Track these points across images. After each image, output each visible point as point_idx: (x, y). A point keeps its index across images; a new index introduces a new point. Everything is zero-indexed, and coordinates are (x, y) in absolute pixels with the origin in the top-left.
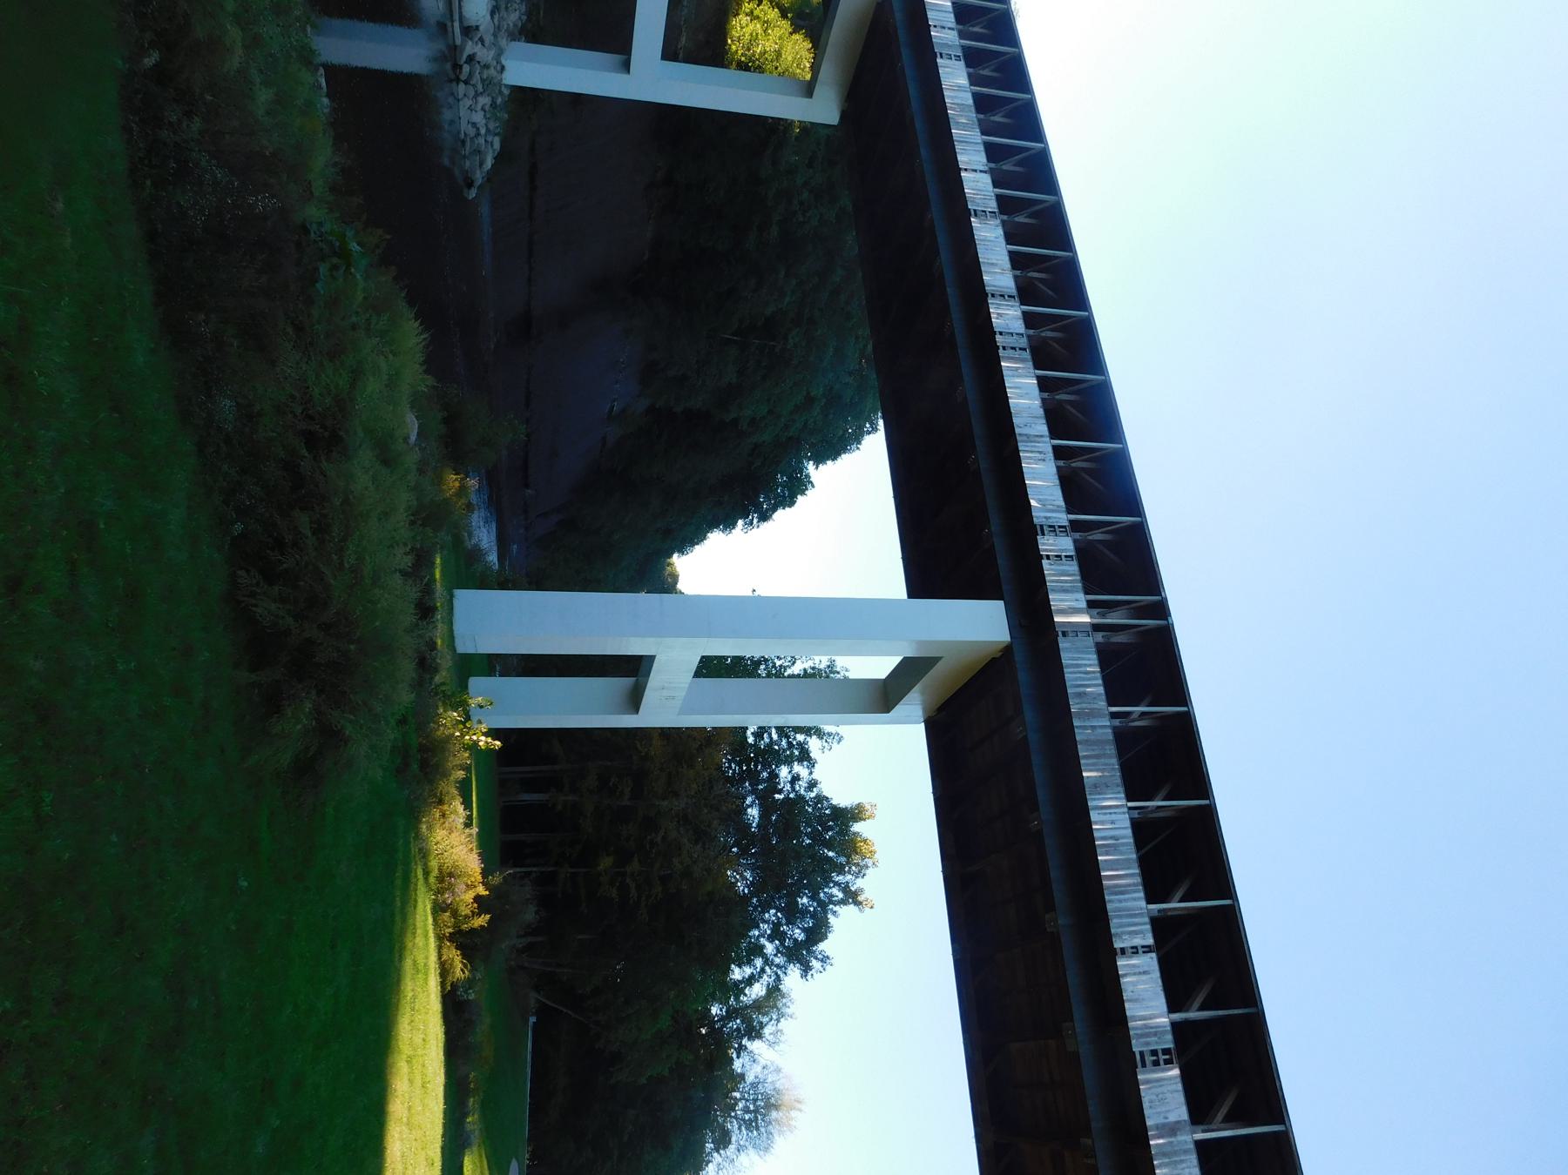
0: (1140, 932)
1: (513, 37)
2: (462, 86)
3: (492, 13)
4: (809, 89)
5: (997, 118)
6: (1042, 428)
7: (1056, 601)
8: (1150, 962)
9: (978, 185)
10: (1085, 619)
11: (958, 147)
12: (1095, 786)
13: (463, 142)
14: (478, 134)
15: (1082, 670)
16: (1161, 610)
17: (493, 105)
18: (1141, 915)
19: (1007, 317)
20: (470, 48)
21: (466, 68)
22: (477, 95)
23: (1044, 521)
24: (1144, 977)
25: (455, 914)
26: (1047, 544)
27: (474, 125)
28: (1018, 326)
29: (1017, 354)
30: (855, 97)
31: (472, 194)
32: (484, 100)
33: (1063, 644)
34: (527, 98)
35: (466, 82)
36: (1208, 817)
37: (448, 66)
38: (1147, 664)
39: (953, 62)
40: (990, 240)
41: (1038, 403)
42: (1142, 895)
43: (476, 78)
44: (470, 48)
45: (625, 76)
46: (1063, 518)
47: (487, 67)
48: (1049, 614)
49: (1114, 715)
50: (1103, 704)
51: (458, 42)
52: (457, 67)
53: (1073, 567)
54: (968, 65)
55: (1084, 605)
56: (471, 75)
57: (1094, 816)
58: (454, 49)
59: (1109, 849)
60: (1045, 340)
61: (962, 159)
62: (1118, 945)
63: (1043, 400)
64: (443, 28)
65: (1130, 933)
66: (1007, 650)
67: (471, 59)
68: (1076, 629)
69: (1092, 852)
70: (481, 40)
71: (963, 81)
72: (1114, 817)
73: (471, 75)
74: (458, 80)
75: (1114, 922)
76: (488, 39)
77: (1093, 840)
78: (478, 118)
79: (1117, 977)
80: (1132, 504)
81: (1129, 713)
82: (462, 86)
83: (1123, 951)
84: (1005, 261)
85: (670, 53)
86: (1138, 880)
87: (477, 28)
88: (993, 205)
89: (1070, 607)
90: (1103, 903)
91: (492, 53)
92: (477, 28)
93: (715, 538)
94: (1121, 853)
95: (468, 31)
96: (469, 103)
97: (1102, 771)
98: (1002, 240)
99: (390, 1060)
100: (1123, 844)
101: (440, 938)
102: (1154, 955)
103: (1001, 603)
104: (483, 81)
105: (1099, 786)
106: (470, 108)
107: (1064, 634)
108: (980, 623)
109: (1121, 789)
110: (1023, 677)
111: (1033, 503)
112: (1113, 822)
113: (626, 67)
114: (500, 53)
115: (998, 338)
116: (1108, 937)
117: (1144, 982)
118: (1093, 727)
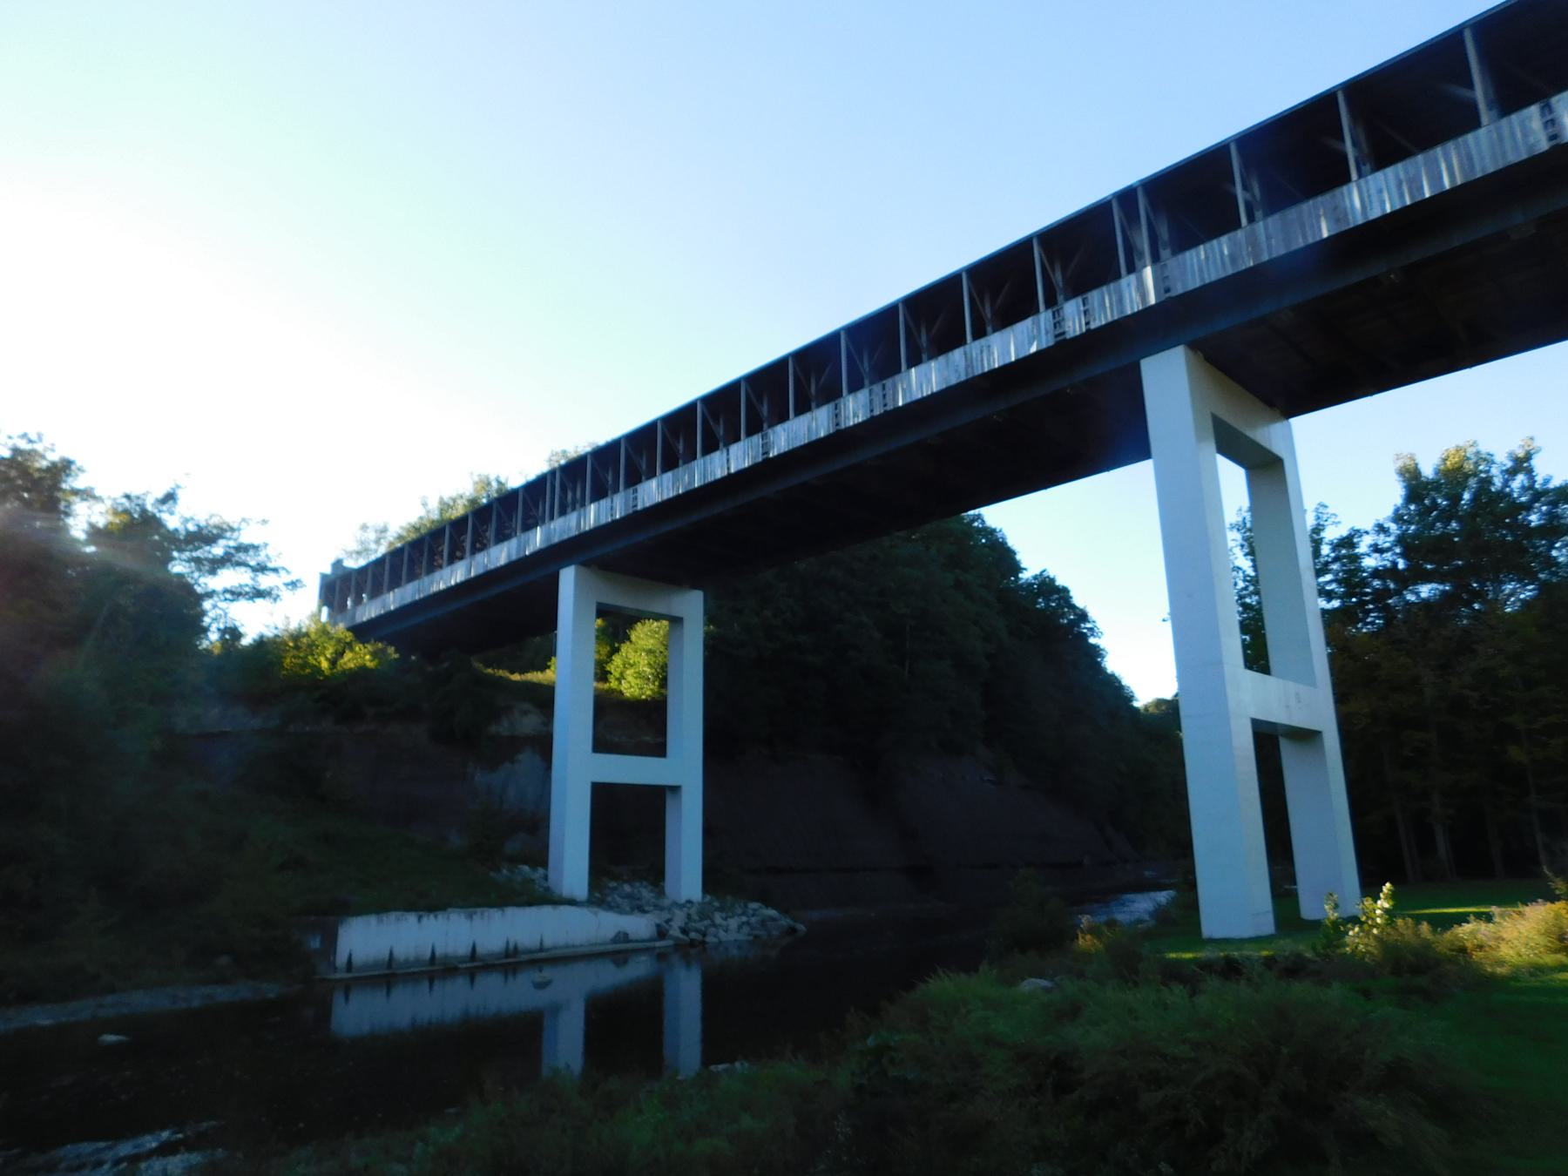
0: (1522, 124)
1: (661, 893)
2: (709, 939)
6: (957, 355)
7: (1132, 305)
9: (739, 457)
10: (1148, 272)
11: (710, 479)
12: (1338, 221)
13: (756, 937)
14: (748, 923)
15: (1207, 262)
16: (1126, 197)
17: (721, 909)
19: (855, 409)
20: (675, 932)
21: (693, 935)
22: (714, 925)
27: (740, 927)
28: (863, 395)
29: (889, 392)
31: (801, 927)
33: (1179, 289)
34: (712, 878)
35: (704, 935)
36: (1359, 88)
37: (693, 951)
38: (1189, 197)
40: (787, 436)
43: (700, 925)
44: (675, 932)
46: (1045, 316)
47: (689, 916)
48: (1148, 312)
50: (1240, 234)
51: (670, 942)
52: (692, 943)
53: (1094, 296)
55: (1132, 277)
56: (697, 931)
57: (1375, 213)
59: (1415, 185)
62: (1544, 145)
64: (661, 956)
65: (1525, 135)
66: (1193, 346)
69: (1420, 206)
70: (668, 921)
71: (653, 483)
72: (1373, 191)
73: (697, 931)
74: (703, 943)
75: (1513, 158)
76: (666, 915)
77: (1405, 209)
78: (733, 923)
80: (1021, 250)
83: (1553, 137)
84: (805, 419)
85: (660, 750)
86: (1451, 145)
88: (756, 439)
89: (1141, 289)
90: (1488, 178)
91: (677, 912)
92: (658, 926)
93: (1111, 664)
95: (661, 933)
96: (722, 933)
97: (1318, 218)
98: (786, 425)
100: (1406, 172)
102: (1554, 100)
104: (701, 919)
105: (1337, 214)
106: (726, 931)
107: (1167, 290)
108: (1169, 383)
109: (1337, 192)
111: (1033, 349)
112: (1380, 191)
113: (675, 789)
115: (877, 412)
118: (1268, 238)
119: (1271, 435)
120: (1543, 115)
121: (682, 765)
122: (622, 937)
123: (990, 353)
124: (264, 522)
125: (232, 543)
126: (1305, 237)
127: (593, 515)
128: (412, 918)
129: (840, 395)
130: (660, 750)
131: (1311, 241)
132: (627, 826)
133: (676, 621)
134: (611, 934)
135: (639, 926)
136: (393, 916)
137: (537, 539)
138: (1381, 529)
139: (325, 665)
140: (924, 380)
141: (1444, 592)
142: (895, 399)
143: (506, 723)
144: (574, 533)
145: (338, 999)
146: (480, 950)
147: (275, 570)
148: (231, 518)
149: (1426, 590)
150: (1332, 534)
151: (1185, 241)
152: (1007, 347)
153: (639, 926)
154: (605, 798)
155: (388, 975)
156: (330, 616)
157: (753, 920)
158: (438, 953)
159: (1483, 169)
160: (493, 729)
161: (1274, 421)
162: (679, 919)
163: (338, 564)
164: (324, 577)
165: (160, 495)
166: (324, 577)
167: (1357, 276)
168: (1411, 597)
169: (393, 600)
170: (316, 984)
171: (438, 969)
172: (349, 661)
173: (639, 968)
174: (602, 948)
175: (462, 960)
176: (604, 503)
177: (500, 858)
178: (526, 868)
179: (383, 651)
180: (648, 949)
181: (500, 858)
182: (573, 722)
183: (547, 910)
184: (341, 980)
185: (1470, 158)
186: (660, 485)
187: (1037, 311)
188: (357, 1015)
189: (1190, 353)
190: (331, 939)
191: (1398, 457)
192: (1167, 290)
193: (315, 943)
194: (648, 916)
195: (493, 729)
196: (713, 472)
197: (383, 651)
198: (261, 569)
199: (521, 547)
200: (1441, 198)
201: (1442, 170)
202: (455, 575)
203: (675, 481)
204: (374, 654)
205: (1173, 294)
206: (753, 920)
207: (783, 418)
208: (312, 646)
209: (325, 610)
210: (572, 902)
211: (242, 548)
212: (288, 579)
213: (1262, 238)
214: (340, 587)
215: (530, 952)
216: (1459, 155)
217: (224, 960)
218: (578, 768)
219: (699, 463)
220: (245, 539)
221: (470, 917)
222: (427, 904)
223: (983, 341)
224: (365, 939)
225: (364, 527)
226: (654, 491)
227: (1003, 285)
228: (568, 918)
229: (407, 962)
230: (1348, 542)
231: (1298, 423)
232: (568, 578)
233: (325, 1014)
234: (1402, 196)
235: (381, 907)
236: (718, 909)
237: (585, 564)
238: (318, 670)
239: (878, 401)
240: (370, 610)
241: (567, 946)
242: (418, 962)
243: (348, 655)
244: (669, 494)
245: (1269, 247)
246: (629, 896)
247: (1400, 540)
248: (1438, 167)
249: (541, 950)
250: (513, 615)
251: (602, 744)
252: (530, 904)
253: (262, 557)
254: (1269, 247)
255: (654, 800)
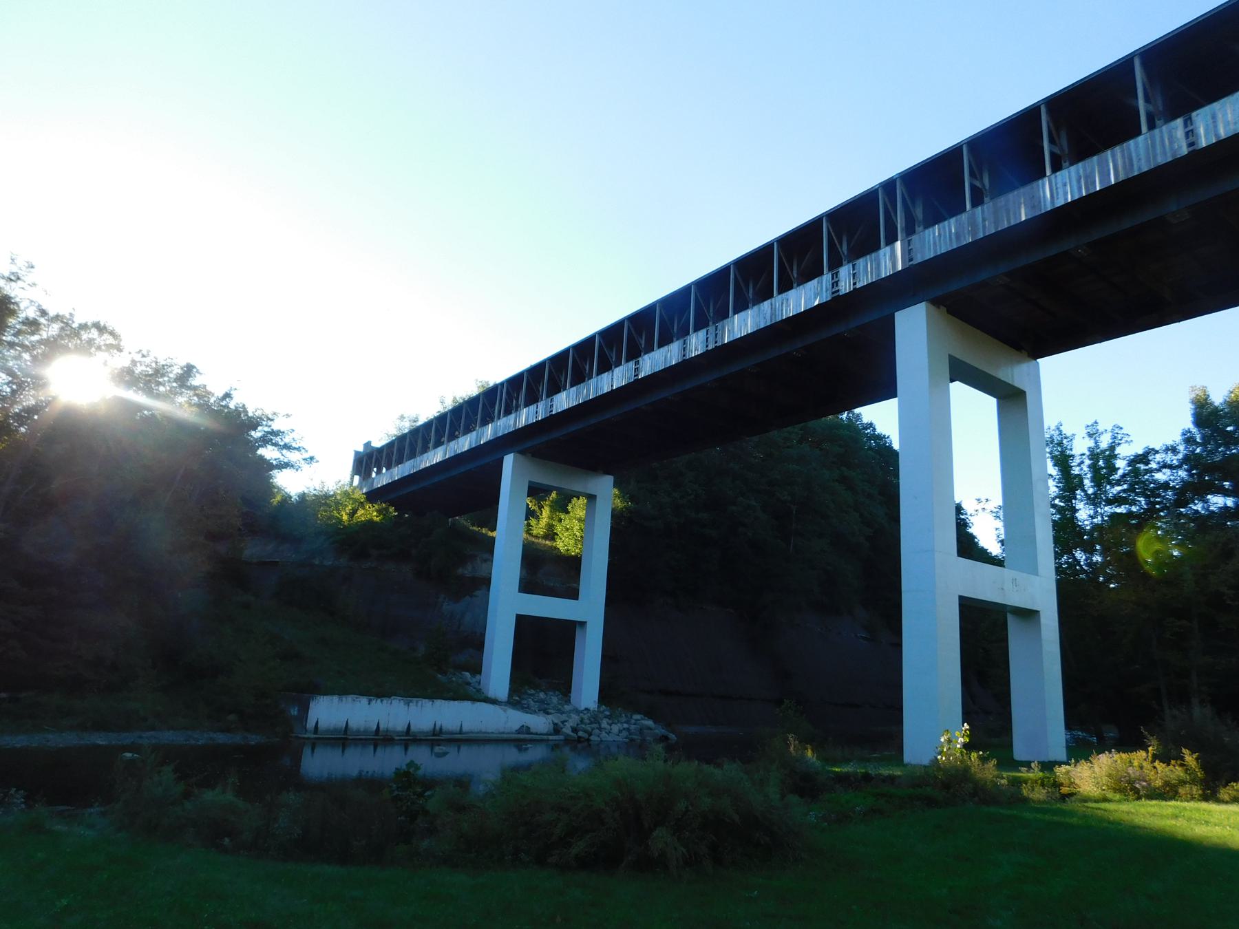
0: (1170, 133)
1: (568, 702)
2: (592, 738)
3: (548, 713)
4: (591, 498)
5: (643, 342)
6: (766, 305)
7: (886, 271)
8: (1201, 118)
9: (619, 377)
10: (898, 245)
11: (600, 393)
12: (1033, 207)
13: (632, 740)
14: (628, 729)
15: (938, 239)
16: (889, 186)
17: (609, 717)
18: (974, 214)
19: (697, 344)
20: (567, 730)
21: (581, 734)
22: (600, 729)
23: (829, 292)
24: (1220, 116)
25: (1183, 782)
26: (845, 287)
27: (620, 731)
28: (702, 334)
29: (720, 333)
30: (595, 466)
31: (672, 736)
32: (604, 724)
33: (918, 259)
34: (607, 694)
35: (590, 734)
37: (579, 746)
38: (935, 184)
39: (554, 403)
41: (1073, 168)
42: (1132, 142)
43: (588, 728)
44: (567, 730)
45: (588, 625)
46: (826, 278)
47: (582, 721)
48: (896, 276)
49: (1152, 126)
50: (964, 217)
51: (562, 737)
52: (579, 740)
53: (861, 262)
54: (791, 288)
55: (888, 249)
56: (585, 731)
57: (1060, 202)
58: (568, 741)
59: (1090, 180)
60: (755, 293)
61: (606, 389)
62: (1185, 151)
63: (1072, 164)
64: (555, 747)
65: (1171, 143)
66: (936, 302)
67: (575, 730)
68: (908, 252)
69: (1092, 197)
70: (563, 722)
71: (563, 395)
72: (1060, 185)
73: (585, 731)
74: (588, 740)
75: (1161, 160)
76: (564, 717)
77: (1081, 199)
78: (615, 728)
79: (1221, 144)
80: (1029, 117)
81: (1052, 155)
82: (592, 738)
83: (1191, 144)
84: (664, 350)
85: (573, 594)
86: (1118, 149)
87: (555, 724)
88: (631, 364)
89: (891, 259)
90: (1143, 175)
91: (573, 715)
92: (555, 724)
93: (981, 544)
94: (1093, 172)
95: (557, 730)
96: (604, 734)
97: (1020, 204)
99: (1180, 837)
100: (1085, 170)
101: (1205, 798)
102: (1194, 114)
103: (897, 314)
104: (591, 723)
105: (1034, 201)
106: (608, 733)
107: (911, 260)
108: (914, 329)
109: (1035, 184)
110: (954, 286)
111: (817, 303)
112: (1065, 185)
113: (583, 624)
114: (577, 711)
115: (710, 348)
116: (1178, 163)
117: (1225, 114)
118: (984, 220)
119: (1016, 374)
120: (1186, 125)
121: (589, 607)
122: (525, 729)
123: (788, 305)
124: (288, 416)
125: (266, 429)
126: (1009, 221)
127: (525, 416)
128: (364, 700)
129: (688, 334)
130: (573, 594)
131: (1013, 223)
132: (543, 650)
133: (591, 498)
134: (517, 727)
135: (540, 723)
136: (350, 698)
137: (488, 433)
138: (1174, 450)
139: (345, 517)
140: (742, 324)
141: (1226, 507)
142: (723, 338)
143: (469, 567)
144: (512, 429)
145: (307, 751)
146: (464, 729)
147: (298, 449)
148: (268, 412)
149: (1217, 501)
150: (1125, 452)
151: (934, 218)
152: (802, 299)
153: (540, 723)
154: (526, 627)
155: (343, 739)
156: (360, 483)
157: (633, 727)
158: (382, 727)
159: (1140, 169)
160: (460, 571)
161: (1019, 362)
162: (573, 720)
163: (368, 445)
164: (357, 453)
165: (221, 395)
166: (357, 453)
167: (1053, 251)
168: (1199, 507)
169: (398, 472)
170: (291, 739)
171: (380, 739)
172: (361, 515)
173: (536, 753)
174: (505, 736)
175: (399, 734)
176: (532, 408)
177: (447, 663)
178: (468, 674)
179: (386, 509)
180: (542, 741)
181: (447, 663)
182: (506, 566)
183: (467, 704)
184: (308, 738)
185: (1131, 160)
186: (568, 396)
187: (821, 273)
188: (319, 764)
189: (932, 308)
190: (305, 709)
191: (1193, 389)
192: (911, 260)
193: (294, 712)
194: (550, 717)
195: (460, 571)
196: (602, 388)
197: (386, 509)
198: (287, 447)
199: (479, 438)
200: (1108, 191)
201: (1107, 169)
202: (436, 456)
203: (578, 393)
204: (379, 512)
205: (914, 262)
206: (633, 727)
207: (649, 349)
208: (338, 503)
209: (357, 478)
210: (494, 702)
211: (276, 433)
212: (307, 456)
213: (980, 220)
214: (367, 461)
215: (451, 733)
216: (1123, 156)
217: (232, 717)
218: (507, 602)
219: (593, 382)
220: (276, 426)
221: (408, 704)
222: (378, 692)
223: (784, 295)
224: (328, 712)
225: (402, 418)
226: (565, 400)
227: (799, 252)
228: (487, 713)
229: (358, 731)
230: (1144, 458)
231: (1045, 363)
232: (509, 461)
233: (297, 759)
234: (1080, 189)
235: (342, 691)
236: (606, 717)
237: (522, 452)
238: (340, 521)
239: (711, 339)
240: (382, 478)
241: (480, 732)
242: (366, 732)
243: (360, 512)
244: (573, 403)
245: (984, 227)
246: (542, 701)
247: (1186, 459)
248: (1108, 166)
249: (461, 732)
250: (471, 486)
251: (528, 586)
252: (454, 700)
253: (287, 440)
254: (984, 227)
255: (567, 631)
